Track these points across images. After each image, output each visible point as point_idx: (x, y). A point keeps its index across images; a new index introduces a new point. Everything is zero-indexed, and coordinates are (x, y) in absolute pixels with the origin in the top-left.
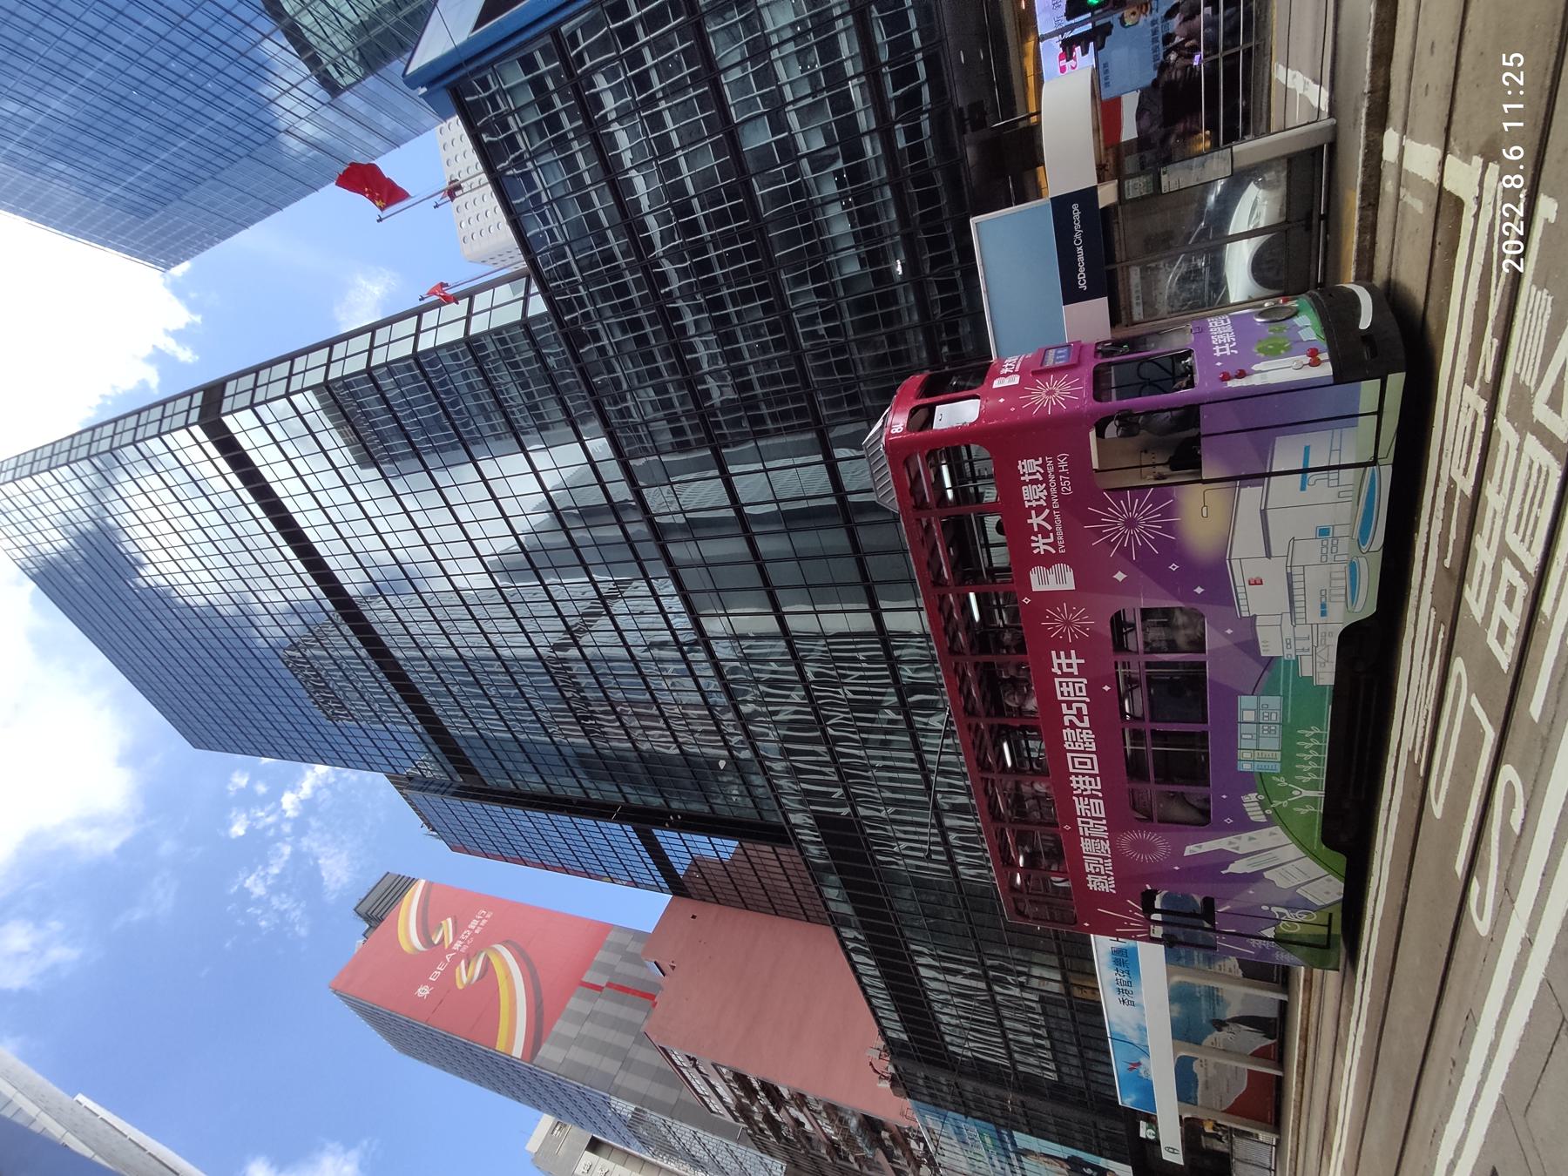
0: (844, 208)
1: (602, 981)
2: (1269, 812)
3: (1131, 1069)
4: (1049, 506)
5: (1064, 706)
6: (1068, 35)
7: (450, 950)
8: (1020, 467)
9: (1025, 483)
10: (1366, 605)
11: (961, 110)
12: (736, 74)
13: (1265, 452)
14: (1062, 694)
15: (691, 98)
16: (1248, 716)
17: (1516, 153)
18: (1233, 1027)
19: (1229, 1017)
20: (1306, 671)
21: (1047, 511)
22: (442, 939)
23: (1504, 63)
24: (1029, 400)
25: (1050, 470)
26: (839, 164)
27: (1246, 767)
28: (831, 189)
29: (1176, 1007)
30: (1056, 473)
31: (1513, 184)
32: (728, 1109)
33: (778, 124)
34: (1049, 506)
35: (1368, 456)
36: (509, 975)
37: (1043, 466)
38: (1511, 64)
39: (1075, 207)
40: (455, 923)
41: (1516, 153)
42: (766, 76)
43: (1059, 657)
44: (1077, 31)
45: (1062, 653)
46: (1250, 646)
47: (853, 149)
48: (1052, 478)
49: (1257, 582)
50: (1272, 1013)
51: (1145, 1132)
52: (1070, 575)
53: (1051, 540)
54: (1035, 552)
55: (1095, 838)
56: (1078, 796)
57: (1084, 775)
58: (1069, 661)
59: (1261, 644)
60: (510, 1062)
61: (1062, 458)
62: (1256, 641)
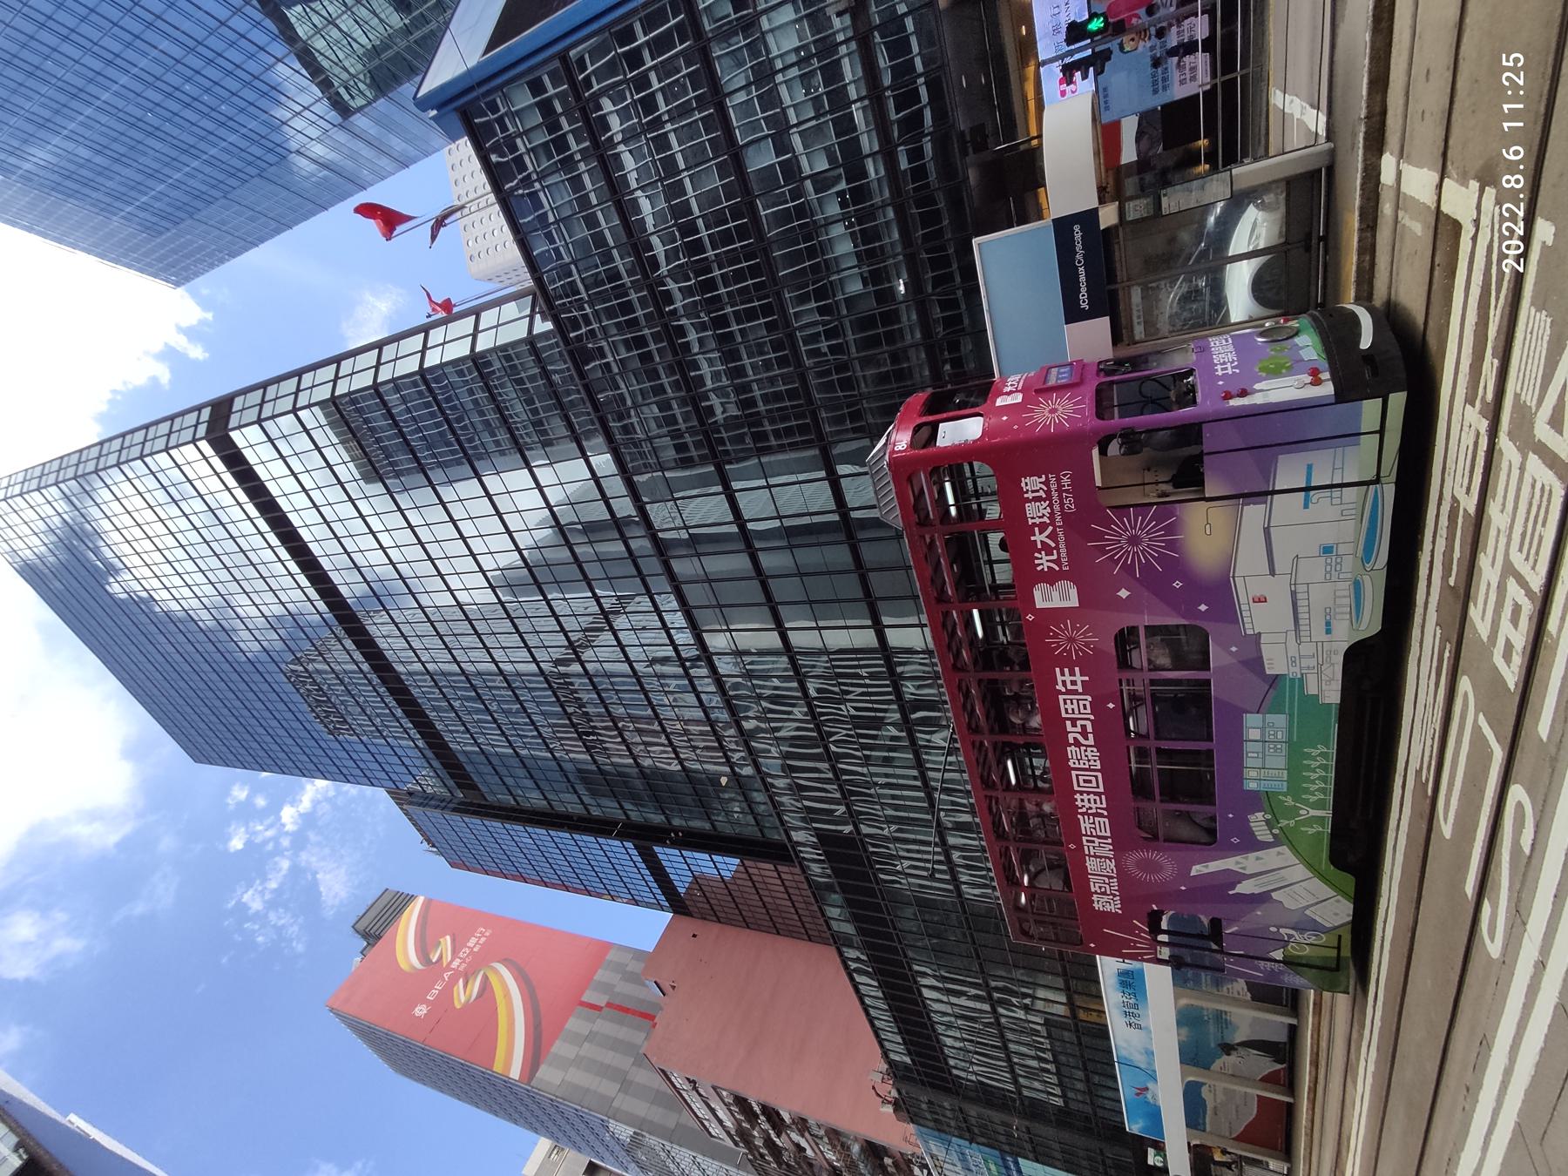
0: (846, 228)
1: (601, 1000)
2: (1276, 831)
3: (1138, 1094)
4: (1053, 523)
5: (1068, 723)
6: (1068, 60)
7: (448, 968)
8: (1023, 485)
9: (1028, 500)
10: (1370, 623)
11: (962, 133)
12: (741, 97)
13: (1268, 471)
14: (1067, 712)
15: (696, 121)
16: (1254, 734)
17: (1516, 153)
18: (1242, 1051)
19: (1238, 1040)
20: (1312, 689)
21: (1050, 528)
22: (441, 957)
23: (1504, 63)
24: (1031, 418)
25: (1054, 487)
26: (843, 185)
27: (1252, 786)
28: (833, 209)
29: (1185, 1031)
30: (1060, 490)
31: (1513, 184)
32: (728, 1133)
33: (782, 146)
34: (1053, 523)
35: (1370, 474)
36: (507, 995)
37: (1046, 483)
38: (1511, 64)
39: (1077, 228)
40: (453, 941)
41: (1516, 153)
42: (770, 99)
43: (1063, 674)
44: (1077, 57)
45: (1066, 670)
46: (1255, 663)
47: (855, 170)
48: (1055, 495)
49: (1261, 600)
50: (1281, 1037)
51: (1152, 1159)
52: (1074, 592)
53: (1055, 557)
54: (1039, 568)
55: (1101, 857)
56: (1083, 814)
57: (1088, 793)
58: (1073, 678)
59: (1266, 662)
60: (507, 1083)
61: (1065, 475)
62: (1260, 659)
